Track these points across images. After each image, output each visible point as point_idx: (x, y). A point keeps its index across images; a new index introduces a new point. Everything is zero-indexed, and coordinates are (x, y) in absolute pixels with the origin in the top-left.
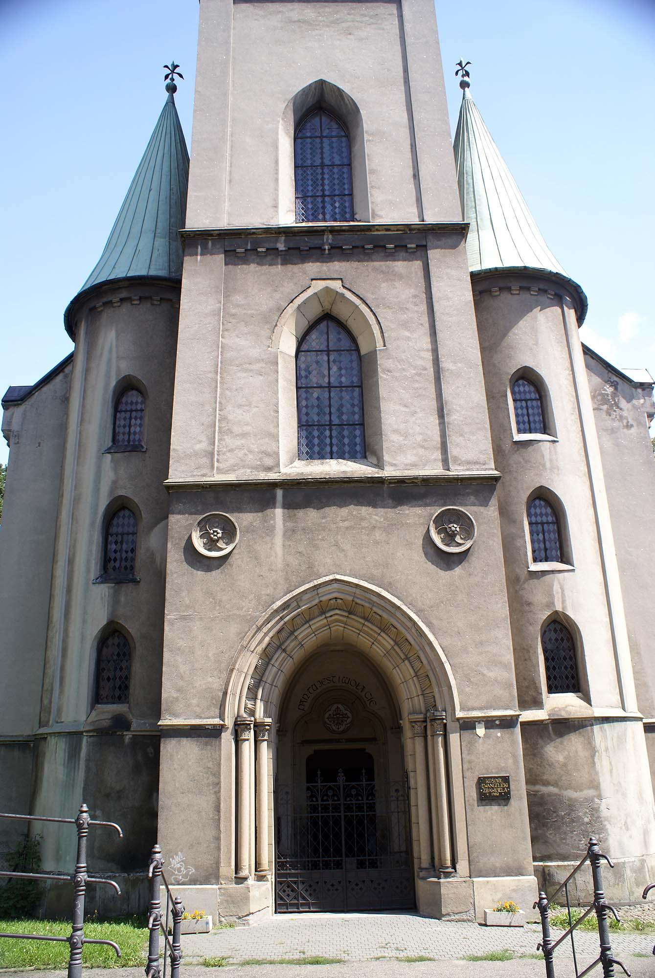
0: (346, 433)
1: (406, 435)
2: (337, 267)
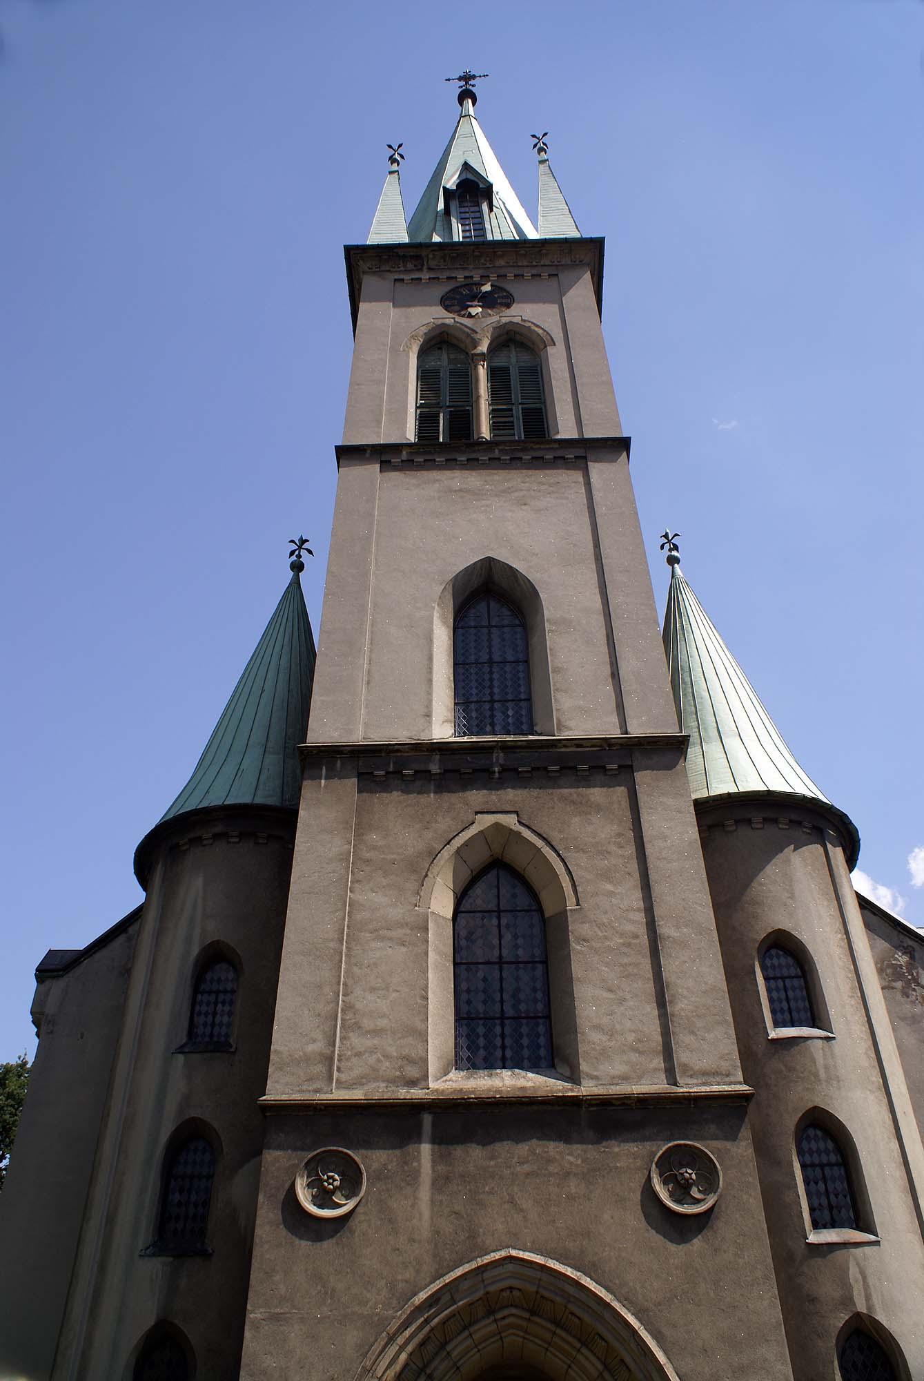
0: (525, 1030)
1: (612, 1034)
2: (511, 795)
